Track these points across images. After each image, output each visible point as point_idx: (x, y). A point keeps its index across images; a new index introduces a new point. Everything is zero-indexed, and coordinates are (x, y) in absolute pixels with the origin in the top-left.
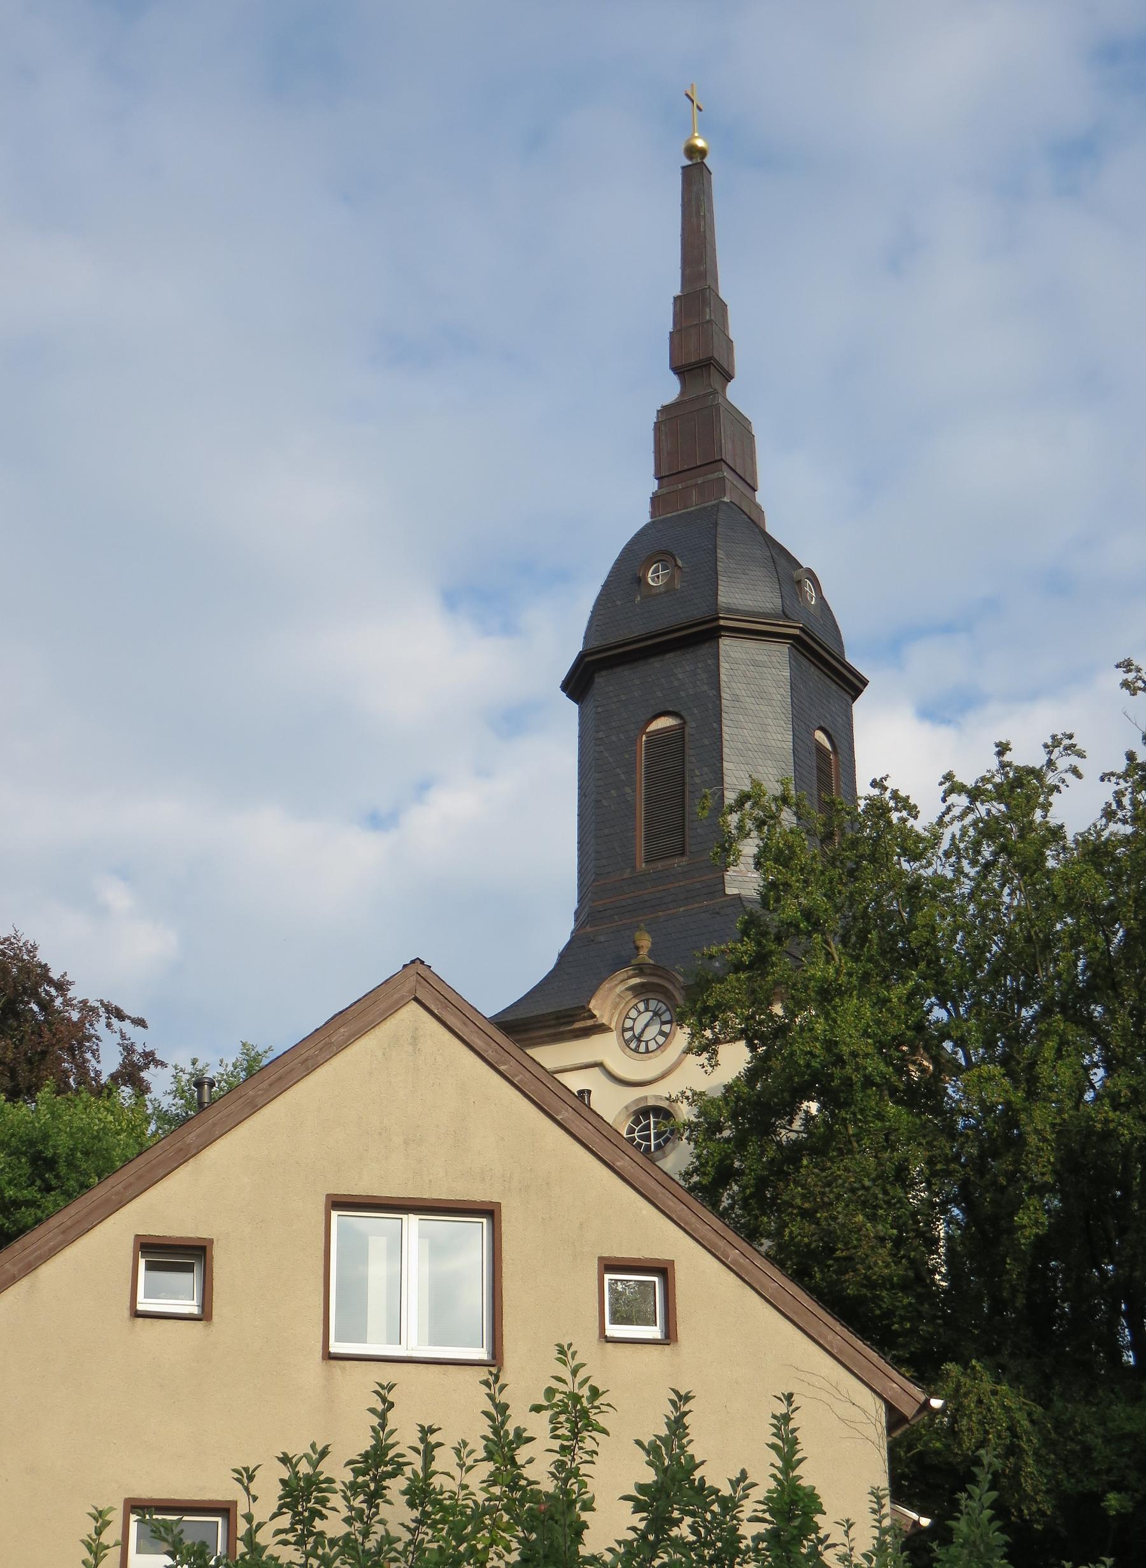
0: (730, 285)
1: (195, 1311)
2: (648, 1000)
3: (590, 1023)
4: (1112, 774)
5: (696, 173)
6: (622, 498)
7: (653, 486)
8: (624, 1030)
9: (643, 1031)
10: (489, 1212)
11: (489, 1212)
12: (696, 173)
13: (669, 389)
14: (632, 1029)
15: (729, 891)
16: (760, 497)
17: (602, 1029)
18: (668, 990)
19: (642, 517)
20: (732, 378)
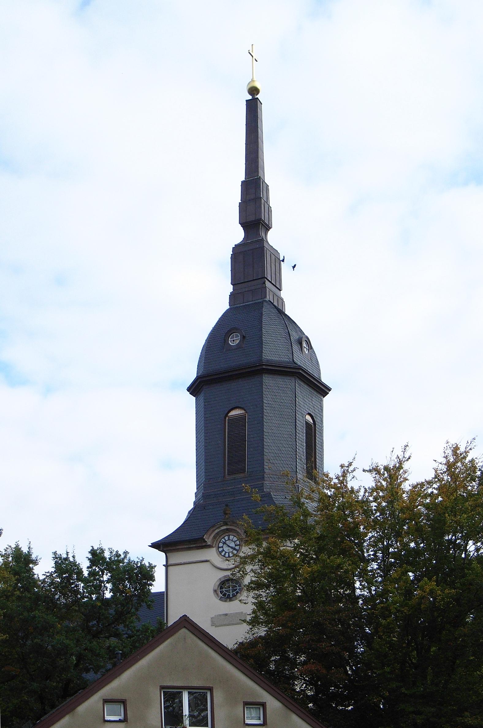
0: (271, 175)
1: (262, 723)
2: (229, 535)
3: (204, 544)
4: (407, 460)
5: (253, 108)
6: (212, 297)
7: (230, 288)
8: (219, 547)
9: (231, 547)
10: (123, 702)
11: (123, 702)
12: (253, 108)
13: (238, 235)
14: (229, 539)
15: (265, 490)
16: (283, 294)
17: (210, 546)
18: (238, 532)
19: (223, 305)
20: (270, 228)
